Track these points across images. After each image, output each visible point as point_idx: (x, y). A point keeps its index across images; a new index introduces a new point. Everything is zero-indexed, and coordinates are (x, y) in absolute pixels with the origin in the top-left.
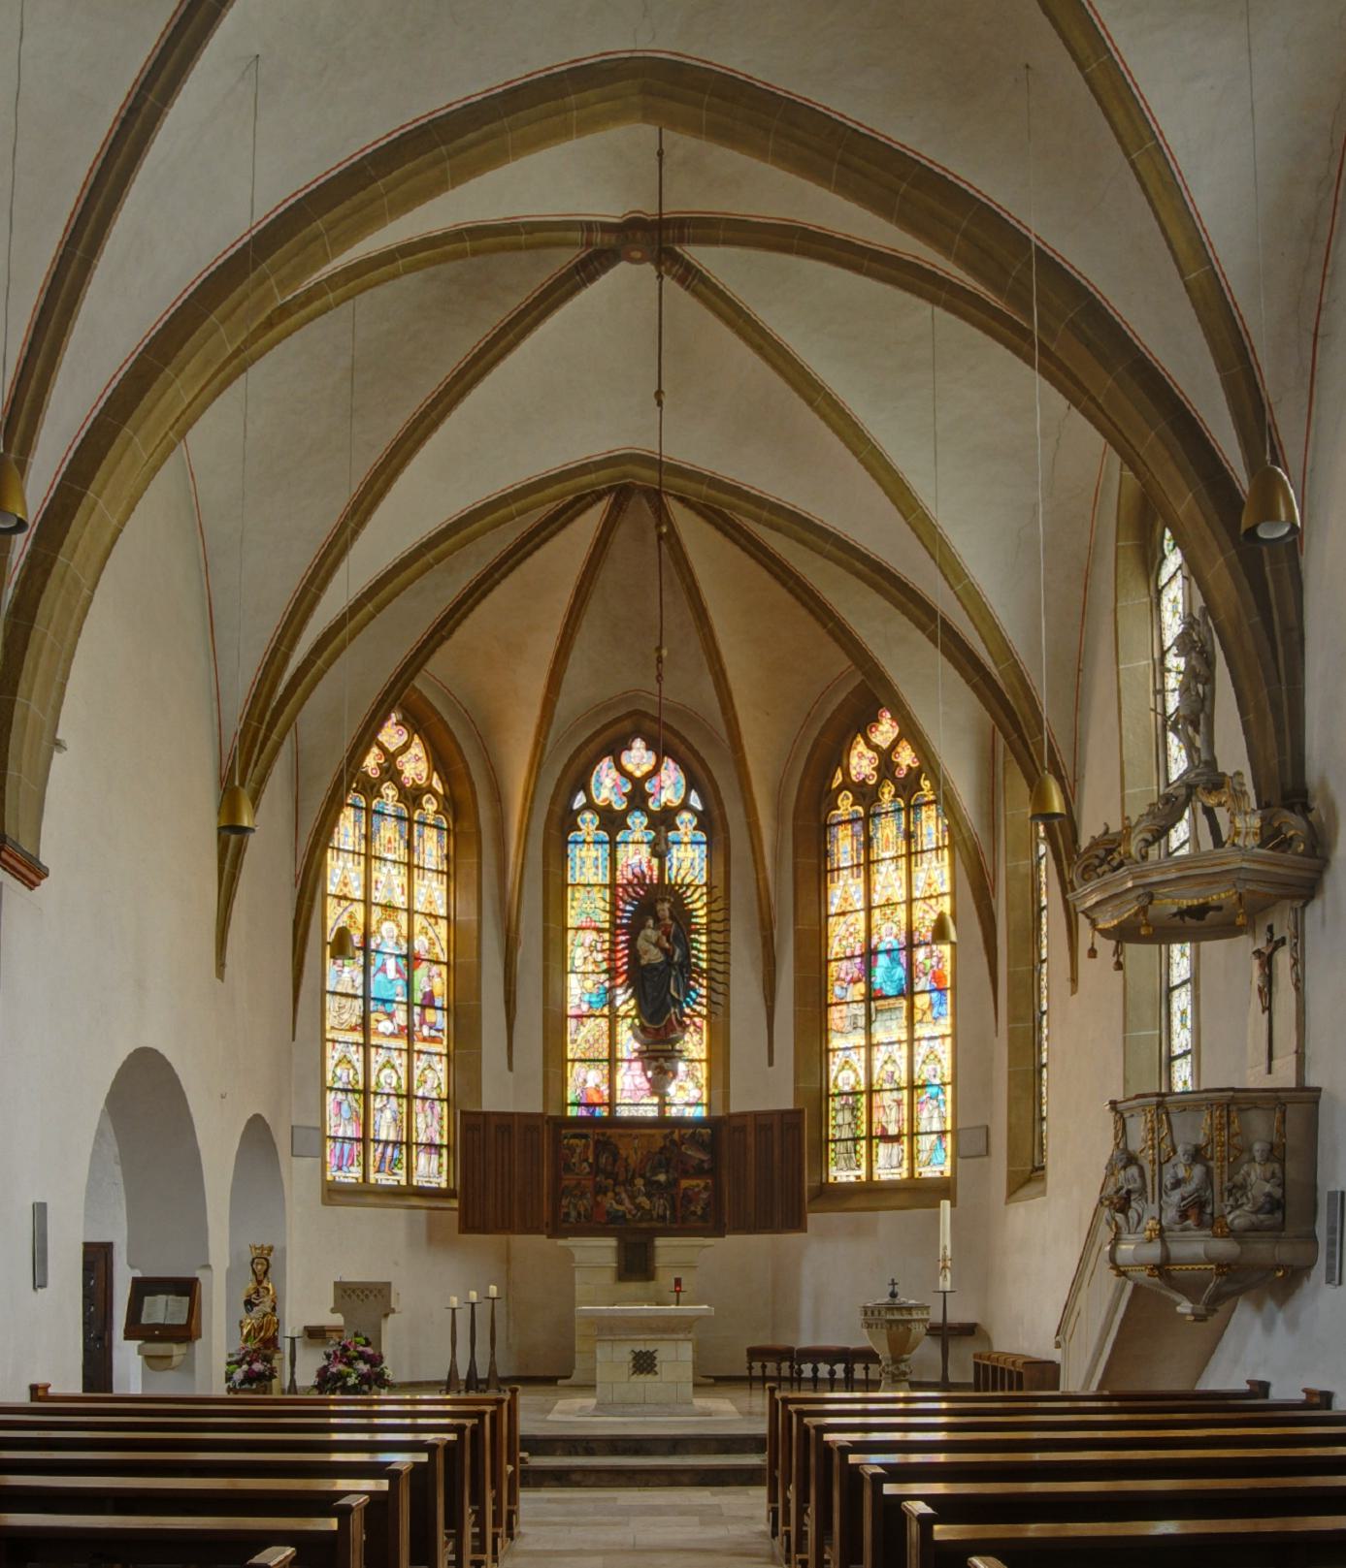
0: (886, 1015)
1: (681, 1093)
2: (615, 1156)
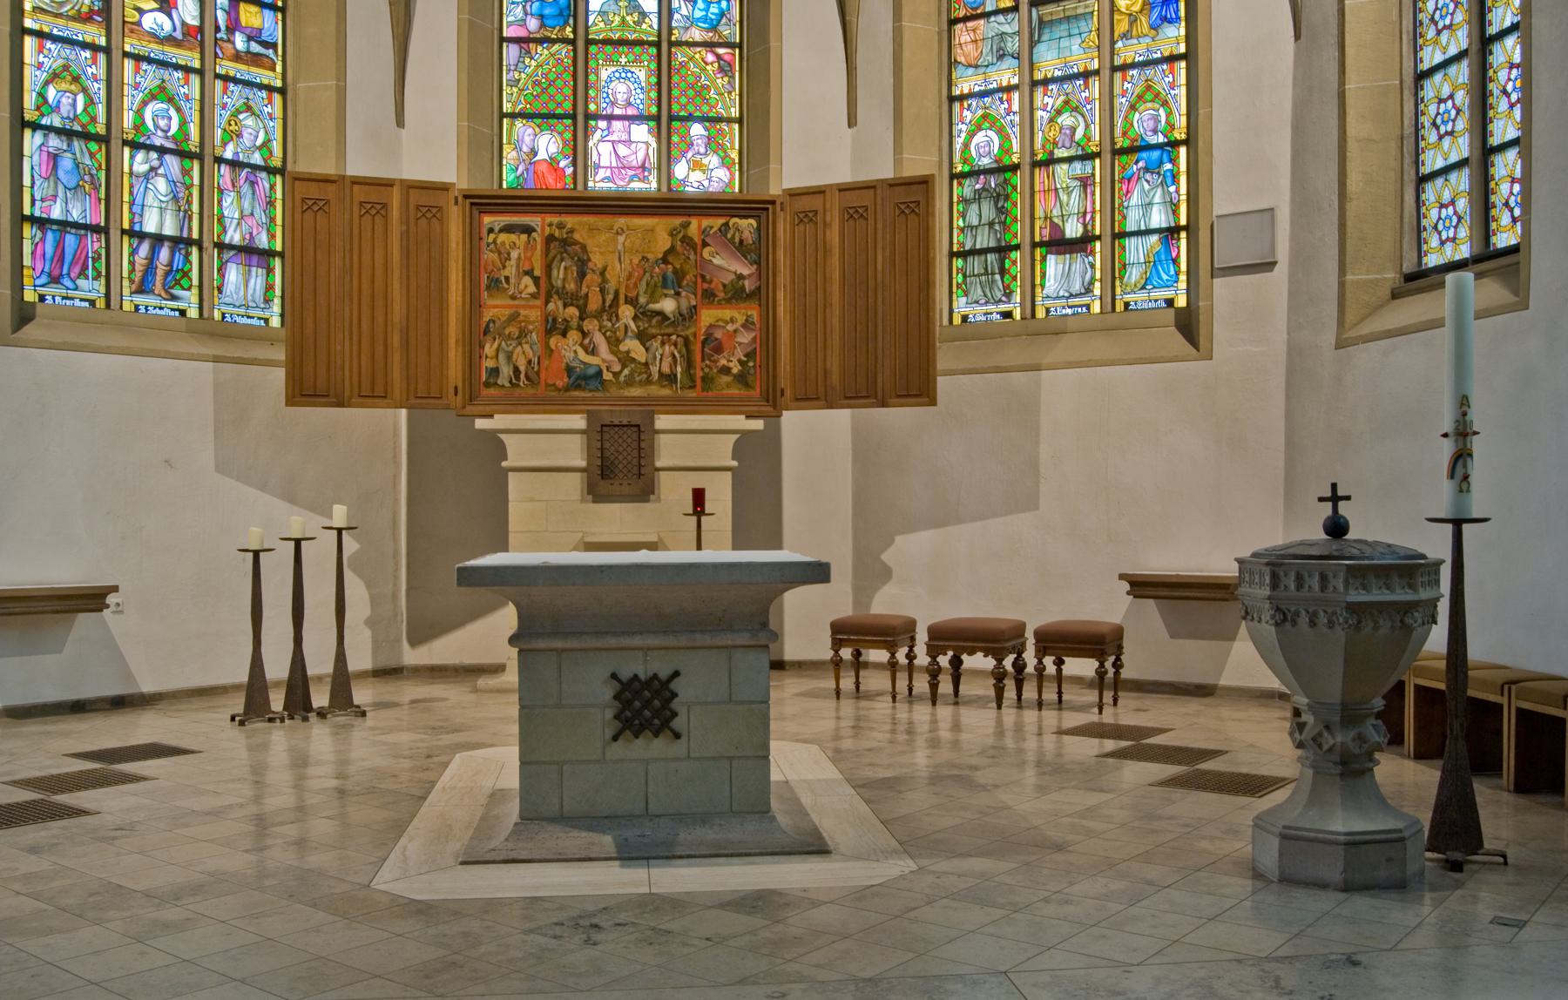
0: (1061, 30)
1: (697, 176)
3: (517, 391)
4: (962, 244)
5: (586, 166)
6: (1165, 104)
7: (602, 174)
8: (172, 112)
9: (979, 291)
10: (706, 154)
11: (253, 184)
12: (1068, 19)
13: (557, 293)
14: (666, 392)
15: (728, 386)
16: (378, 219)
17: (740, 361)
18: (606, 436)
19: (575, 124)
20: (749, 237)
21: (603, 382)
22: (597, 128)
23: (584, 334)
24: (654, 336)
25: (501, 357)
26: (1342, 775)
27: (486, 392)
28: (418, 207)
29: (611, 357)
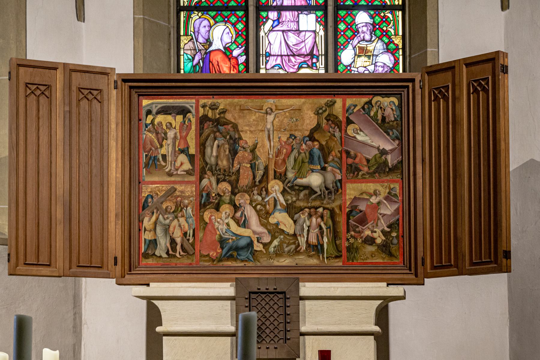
1: (362, 62)
2: (234, 146)
3: (174, 261)
7: (272, 61)
10: (370, 41)
13: (211, 170)
14: (314, 261)
15: (372, 255)
16: (43, 99)
17: (383, 232)
19: (247, 15)
20: (391, 114)
21: (254, 253)
22: (267, 18)
23: (236, 208)
24: (302, 209)
25: (159, 229)
26: (167, 140)
27: (144, 262)
28: (80, 89)
29: (261, 229)
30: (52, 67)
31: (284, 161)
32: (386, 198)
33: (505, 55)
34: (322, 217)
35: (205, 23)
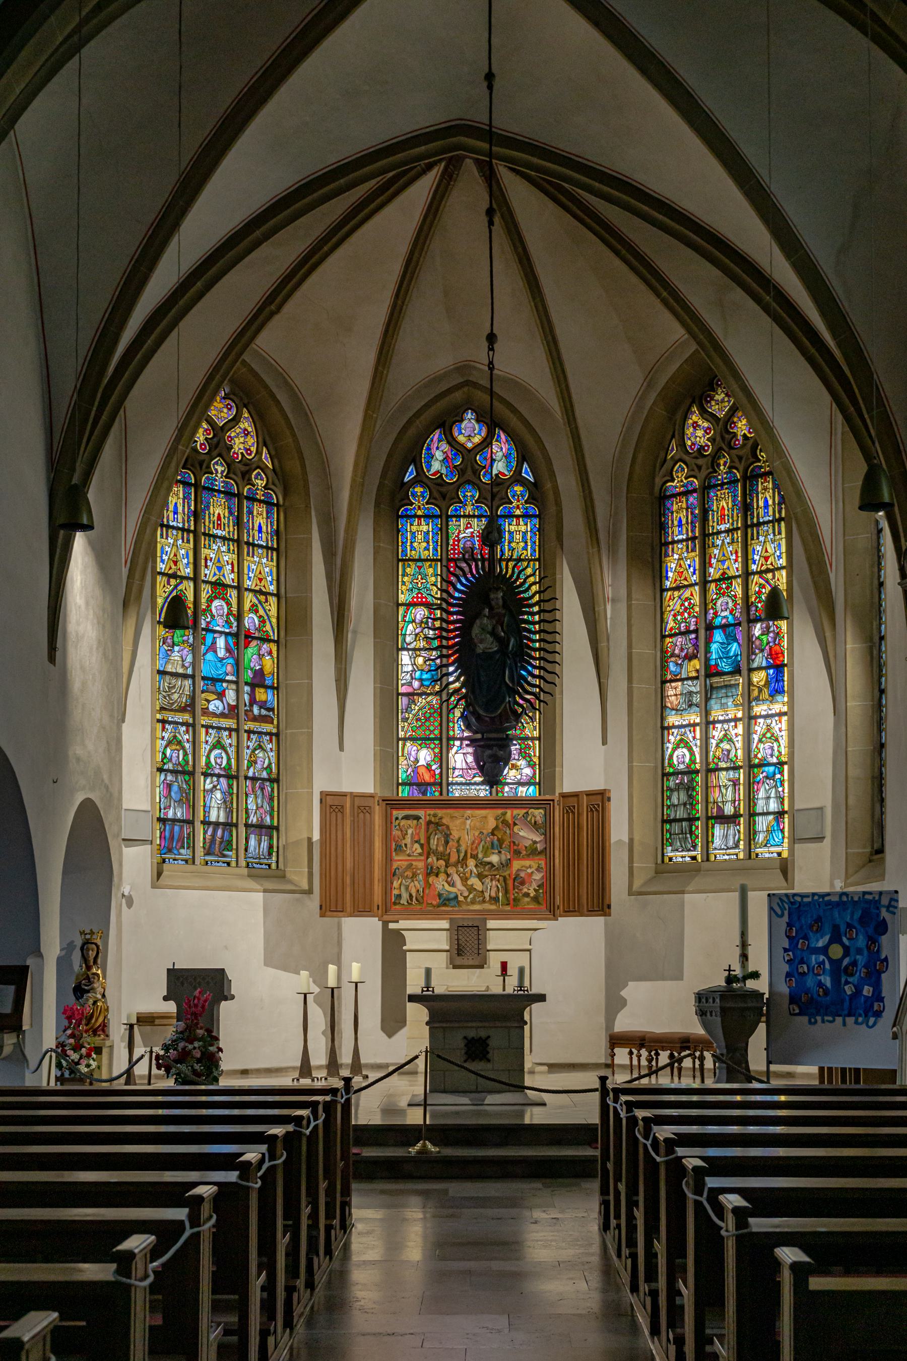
3: (411, 907)
4: (668, 815)
5: (448, 769)
6: (777, 740)
7: (457, 773)
8: (224, 755)
9: (678, 844)
10: (518, 760)
11: (262, 789)
12: (726, 686)
15: (528, 903)
17: (535, 890)
18: (460, 933)
19: (441, 743)
21: (458, 902)
23: (448, 875)
24: (486, 876)
27: (394, 907)
29: (463, 888)
30: (344, 795)
31: (476, 848)
32: (537, 870)
33: (609, 791)
34: (499, 881)
35: (415, 748)
